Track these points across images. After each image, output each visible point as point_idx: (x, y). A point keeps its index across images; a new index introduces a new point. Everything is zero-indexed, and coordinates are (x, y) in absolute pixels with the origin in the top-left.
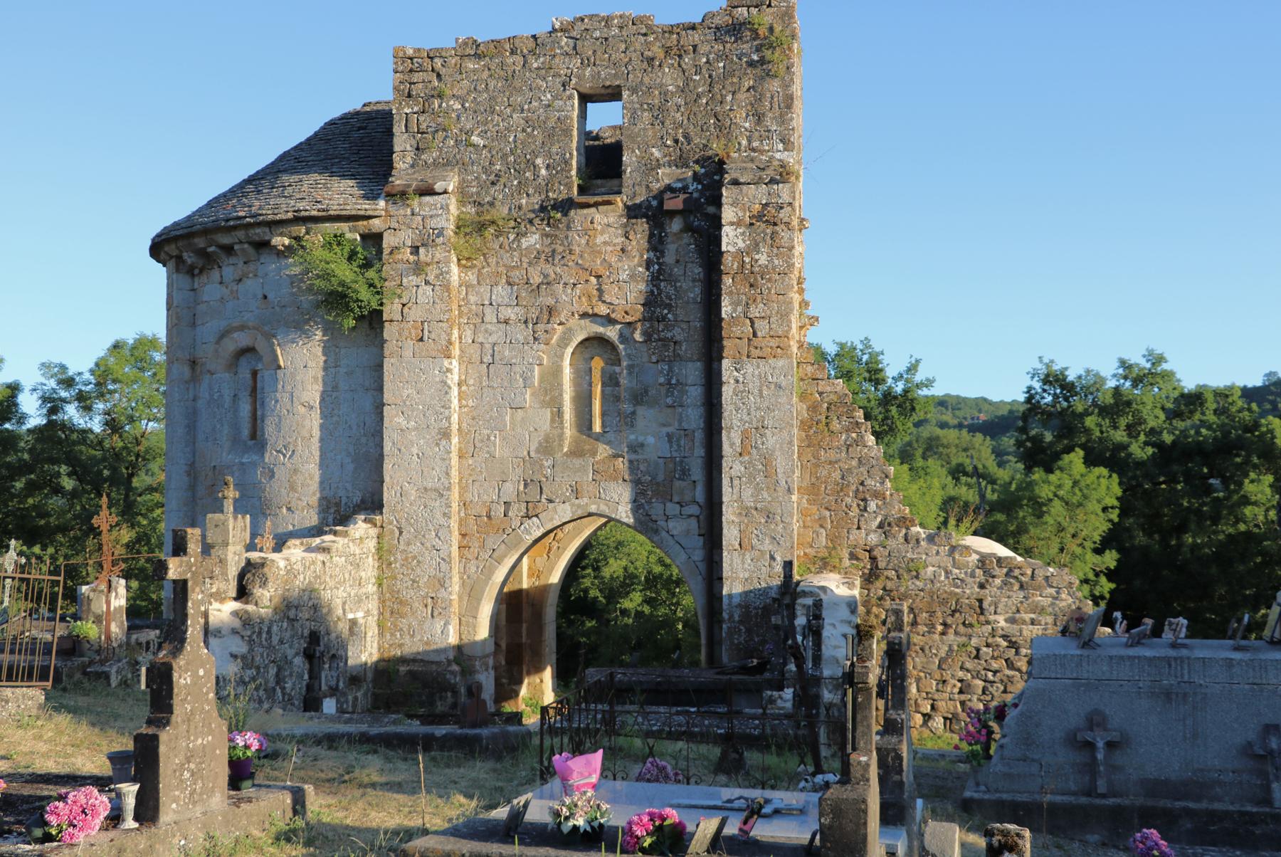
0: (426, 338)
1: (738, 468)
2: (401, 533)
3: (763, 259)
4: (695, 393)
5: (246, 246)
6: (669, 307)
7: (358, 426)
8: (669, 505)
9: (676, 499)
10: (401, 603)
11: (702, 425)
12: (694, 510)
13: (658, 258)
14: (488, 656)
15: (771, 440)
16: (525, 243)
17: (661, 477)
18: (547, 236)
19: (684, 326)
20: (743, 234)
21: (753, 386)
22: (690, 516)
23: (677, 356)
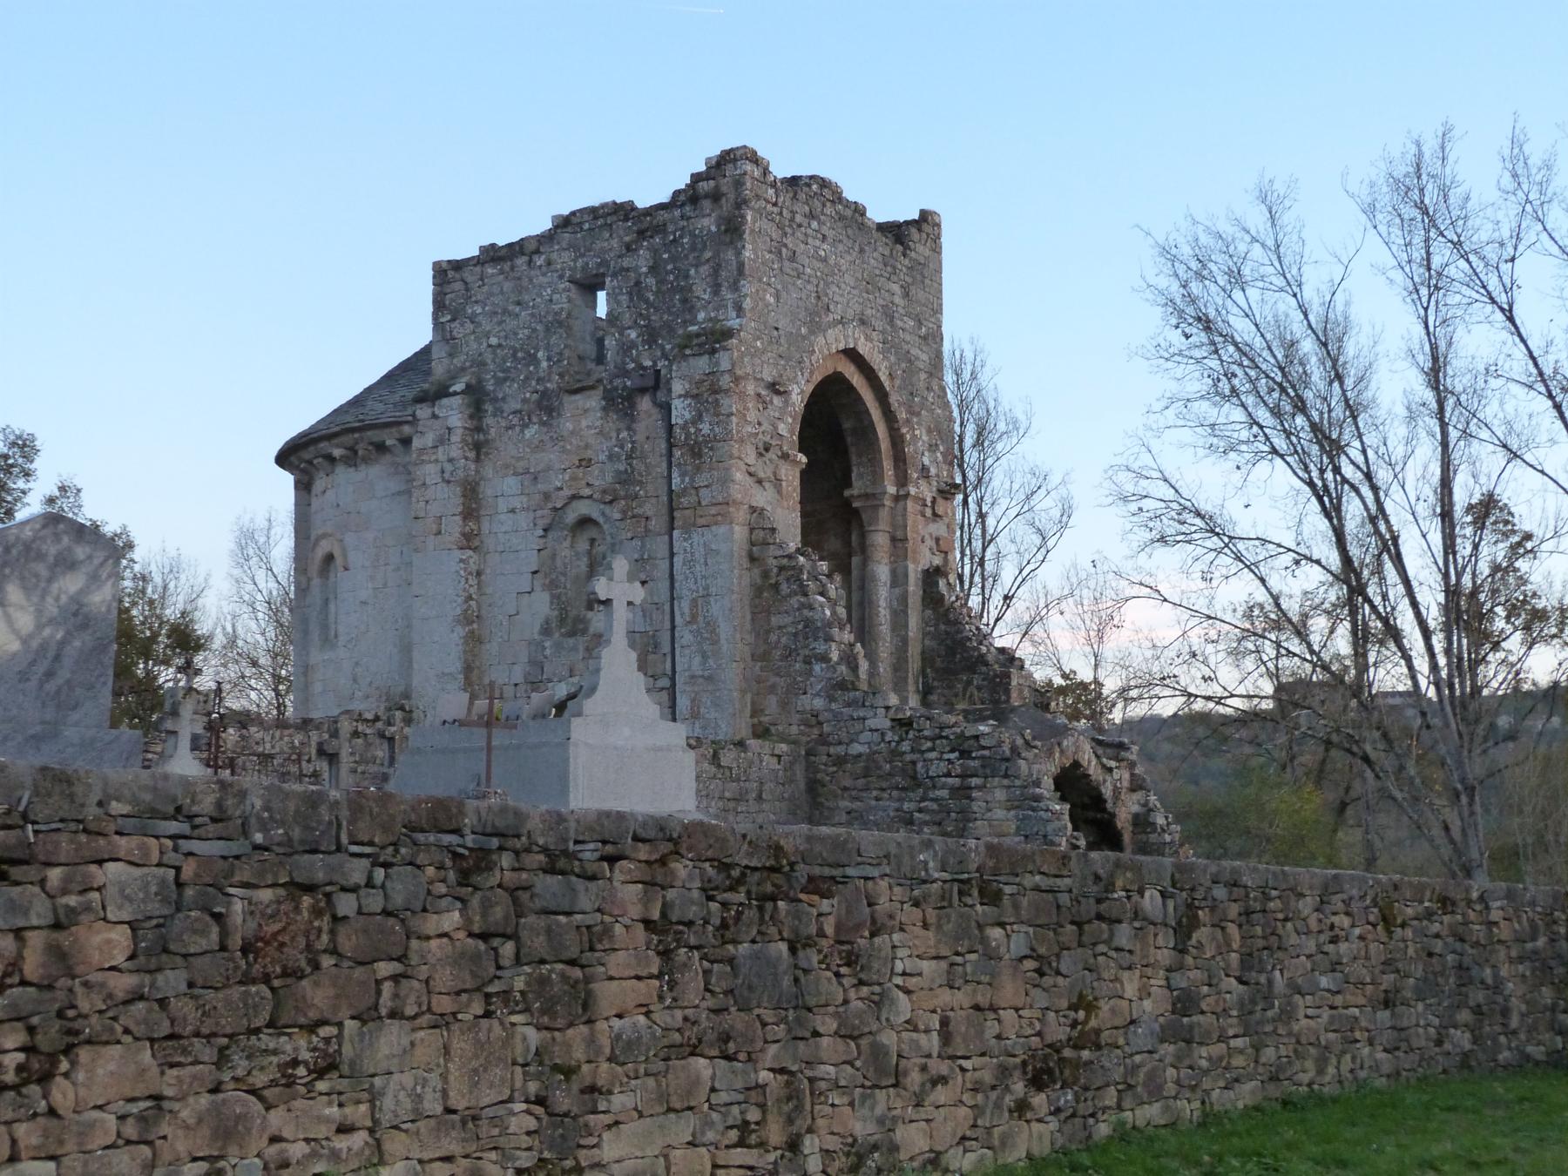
3: (705, 428)
6: (640, 483)
15: (715, 609)
16: (528, 433)
19: (654, 500)
21: (699, 553)
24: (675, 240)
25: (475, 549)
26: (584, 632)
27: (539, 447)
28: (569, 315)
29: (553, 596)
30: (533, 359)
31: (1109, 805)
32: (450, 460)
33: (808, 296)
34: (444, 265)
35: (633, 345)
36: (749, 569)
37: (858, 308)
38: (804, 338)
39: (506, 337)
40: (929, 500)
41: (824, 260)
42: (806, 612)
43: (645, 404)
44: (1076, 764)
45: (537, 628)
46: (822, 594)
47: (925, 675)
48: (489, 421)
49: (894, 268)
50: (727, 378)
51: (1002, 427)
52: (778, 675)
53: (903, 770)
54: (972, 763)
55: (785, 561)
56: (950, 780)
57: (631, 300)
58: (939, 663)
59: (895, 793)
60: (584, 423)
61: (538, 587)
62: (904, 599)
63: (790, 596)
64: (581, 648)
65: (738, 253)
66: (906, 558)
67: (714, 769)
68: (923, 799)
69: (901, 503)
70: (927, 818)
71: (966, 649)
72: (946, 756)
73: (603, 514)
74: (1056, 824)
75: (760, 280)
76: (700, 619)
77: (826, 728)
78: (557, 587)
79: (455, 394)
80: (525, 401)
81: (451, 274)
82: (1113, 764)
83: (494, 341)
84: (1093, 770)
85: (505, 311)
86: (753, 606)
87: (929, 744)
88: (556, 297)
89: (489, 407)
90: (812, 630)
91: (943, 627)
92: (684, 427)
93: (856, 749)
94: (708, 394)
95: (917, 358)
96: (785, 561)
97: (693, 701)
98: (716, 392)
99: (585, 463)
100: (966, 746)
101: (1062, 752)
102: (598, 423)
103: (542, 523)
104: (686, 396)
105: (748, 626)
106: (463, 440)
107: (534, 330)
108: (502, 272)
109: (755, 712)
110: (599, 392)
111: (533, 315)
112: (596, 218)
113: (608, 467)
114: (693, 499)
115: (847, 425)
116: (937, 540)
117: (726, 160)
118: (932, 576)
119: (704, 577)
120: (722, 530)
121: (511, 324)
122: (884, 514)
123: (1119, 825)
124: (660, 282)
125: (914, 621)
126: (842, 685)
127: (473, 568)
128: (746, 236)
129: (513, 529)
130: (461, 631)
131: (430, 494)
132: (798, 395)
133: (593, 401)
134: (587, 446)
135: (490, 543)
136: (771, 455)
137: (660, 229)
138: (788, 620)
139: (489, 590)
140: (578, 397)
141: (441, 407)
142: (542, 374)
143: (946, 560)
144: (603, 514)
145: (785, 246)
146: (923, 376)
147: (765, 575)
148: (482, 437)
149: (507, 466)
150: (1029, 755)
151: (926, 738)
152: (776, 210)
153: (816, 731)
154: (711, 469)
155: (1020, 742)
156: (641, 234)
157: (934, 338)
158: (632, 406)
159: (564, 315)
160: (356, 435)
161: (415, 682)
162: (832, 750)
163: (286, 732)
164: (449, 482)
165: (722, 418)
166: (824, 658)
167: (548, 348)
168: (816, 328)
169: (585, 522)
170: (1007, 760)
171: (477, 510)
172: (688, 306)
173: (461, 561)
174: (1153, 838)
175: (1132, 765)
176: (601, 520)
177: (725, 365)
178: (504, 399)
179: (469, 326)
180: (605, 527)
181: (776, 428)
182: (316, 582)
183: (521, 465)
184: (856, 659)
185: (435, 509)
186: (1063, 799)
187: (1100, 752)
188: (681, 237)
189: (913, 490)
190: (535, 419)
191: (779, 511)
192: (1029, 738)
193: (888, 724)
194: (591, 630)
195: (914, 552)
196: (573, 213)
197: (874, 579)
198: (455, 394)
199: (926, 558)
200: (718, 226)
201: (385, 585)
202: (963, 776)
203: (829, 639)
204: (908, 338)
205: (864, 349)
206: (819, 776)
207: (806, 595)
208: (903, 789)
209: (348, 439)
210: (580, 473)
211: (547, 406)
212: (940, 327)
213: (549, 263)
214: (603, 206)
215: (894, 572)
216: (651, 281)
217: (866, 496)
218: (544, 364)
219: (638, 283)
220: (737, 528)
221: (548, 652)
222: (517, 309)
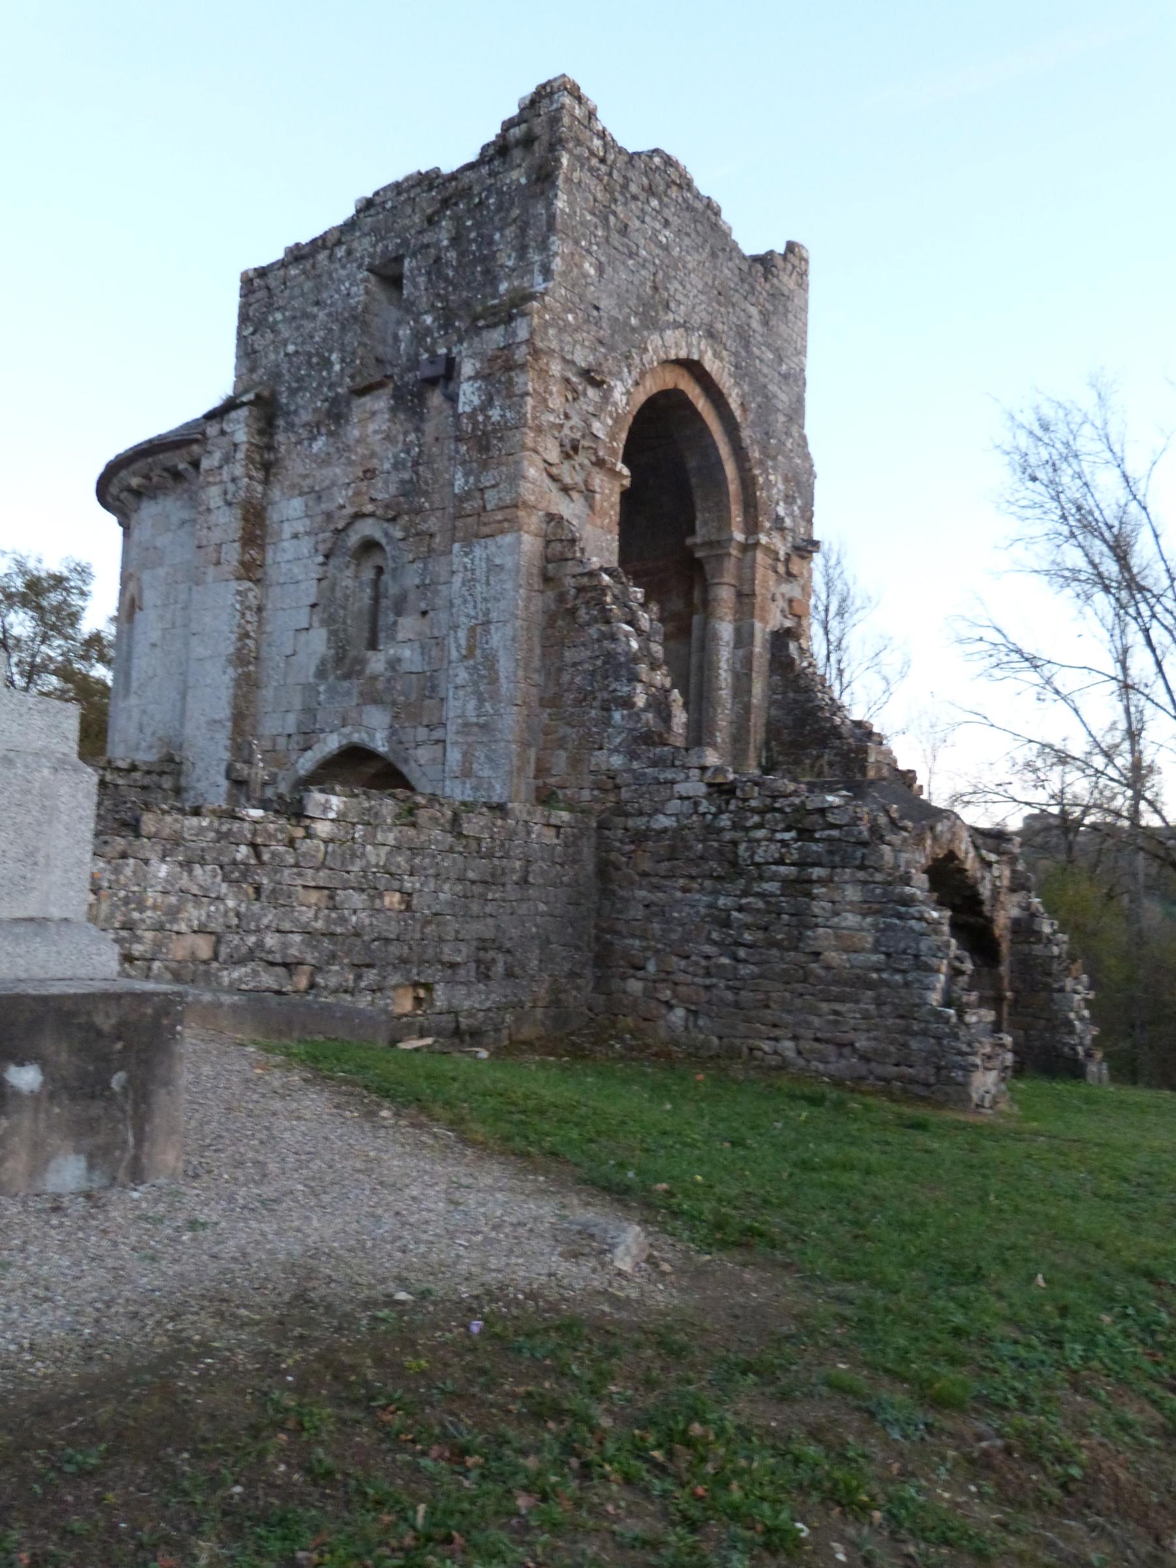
6: (426, 494)
15: (497, 639)
24: (480, 203)
25: (258, 582)
26: (360, 673)
27: (325, 461)
28: (366, 309)
30: (327, 363)
31: (986, 908)
32: (234, 480)
33: (642, 284)
34: (251, 274)
35: (428, 331)
36: (542, 592)
37: (707, 319)
38: (633, 330)
39: (303, 343)
40: (782, 556)
41: (666, 248)
42: (607, 644)
43: (436, 399)
44: (951, 856)
45: (312, 670)
46: (629, 623)
47: (769, 749)
48: (280, 437)
49: (753, 288)
50: (524, 349)
51: (858, 603)
52: (569, 724)
53: (719, 851)
54: (814, 847)
55: (585, 581)
56: (782, 869)
57: (430, 280)
58: (786, 736)
59: (708, 883)
61: (316, 624)
62: (748, 661)
63: (589, 624)
64: (355, 692)
65: (549, 204)
66: (752, 616)
67: (450, 839)
68: (745, 893)
69: (750, 554)
70: (749, 919)
71: (818, 720)
72: (779, 836)
73: (387, 534)
74: (935, 940)
75: (577, 242)
76: (478, 652)
77: (625, 794)
79: (243, 404)
80: (316, 410)
81: (257, 282)
82: (992, 857)
84: (970, 863)
86: (545, 638)
87: (756, 818)
89: (281, 422)
90: (620, 667)
91: (791, 695)
92: (472, 416)
93: (662, 821)
94: (501, 371)
95: (775, 396)
96: (585, 581)
97: (465, 754)
98: (510, 369)
99: (369, 474)
100: (808, 822)
101: (935, 839)
102: (384, 427)
103: (322, 548)
105: (536, 663)
107: (330, 330)
108: (304, 272)
109: (542, 770)
110: (388, 390)
112: (399, 194)
114: (476, 504)
115: (692, 463)
116: (790, 601)
117: (544, 94)
118: (782, 638)
119: (485, 600)
120: (508, 539)
121: (309, 325)
122: (730, 565)
123: (997, 932)
124: (462, 254)
125: (758, 688)
126: (649, 738)
127: (254, 602)
128: (560, 182)
129: (294, 555)
130: (231, 672)
131: (213, 518)
132: (625, 395)
133: (381, 402)
134: (373, 454)
135: (273, 574)
136: (582, 458)
137: (465, 193)
138: (585, 654)
139: (268, 628)
141: (229, 421)
142: (334, 379)
143: (799, 625)
145: (615, 213)
146: (782, 419)
147: (561, 598)
148: (272, 456)
149: (293, 486)
150: (895, 839)
151: (754, 811)
152: (603, 168)
153: (612, 797)
154: (499, 464)
155: (882, 820)
156: (445, 203)
157: (796, 381)
160: (150, 460)
162: (630, 823)
165: (514, 398)
166: (627, 703)
167: (342, 350)
168: (651, 323)
169: (369, 546)
170: (865, 844)
171: (263, 538)
172: (491, 278)
173: (239, 593)
174: (1038, 949)
175: (1013, 860)
176: (383, 541)
177: (523, 334)
179: (270, 336)
180: (388, 548)
181: (589, 426)
184: (668, 707)
185: (216, 536)
186: (941, 904)
187: (980, 841)
188: (487, 198)
189: (763, 539)
190: (323, 430)
191: (589, 527)
192: (895, 815)
193: (702, 789)
194: (368, 672)
195: (763, 609)
196: (377, 194)
197: (716, 637)
198: (243, 404)
199: (776, 619)
200: (528, 178)
201: (174, 625)
202: (801, 864)
203: (634, 678)
204: (765, 370)
205: (711, 364)
206: (613, 856)
207: (608, 622)
208: (719, 878)
209: (139, 465)
211: (336, 415)
212: (802, 370)
213: (349, 253)
214: (407, 179)
215: (738, 631)
217: (710, 544)
218: (337, 367)
219: (438, 260)
220: (526, 538)
221: (322, 697)
222: (315, 310)
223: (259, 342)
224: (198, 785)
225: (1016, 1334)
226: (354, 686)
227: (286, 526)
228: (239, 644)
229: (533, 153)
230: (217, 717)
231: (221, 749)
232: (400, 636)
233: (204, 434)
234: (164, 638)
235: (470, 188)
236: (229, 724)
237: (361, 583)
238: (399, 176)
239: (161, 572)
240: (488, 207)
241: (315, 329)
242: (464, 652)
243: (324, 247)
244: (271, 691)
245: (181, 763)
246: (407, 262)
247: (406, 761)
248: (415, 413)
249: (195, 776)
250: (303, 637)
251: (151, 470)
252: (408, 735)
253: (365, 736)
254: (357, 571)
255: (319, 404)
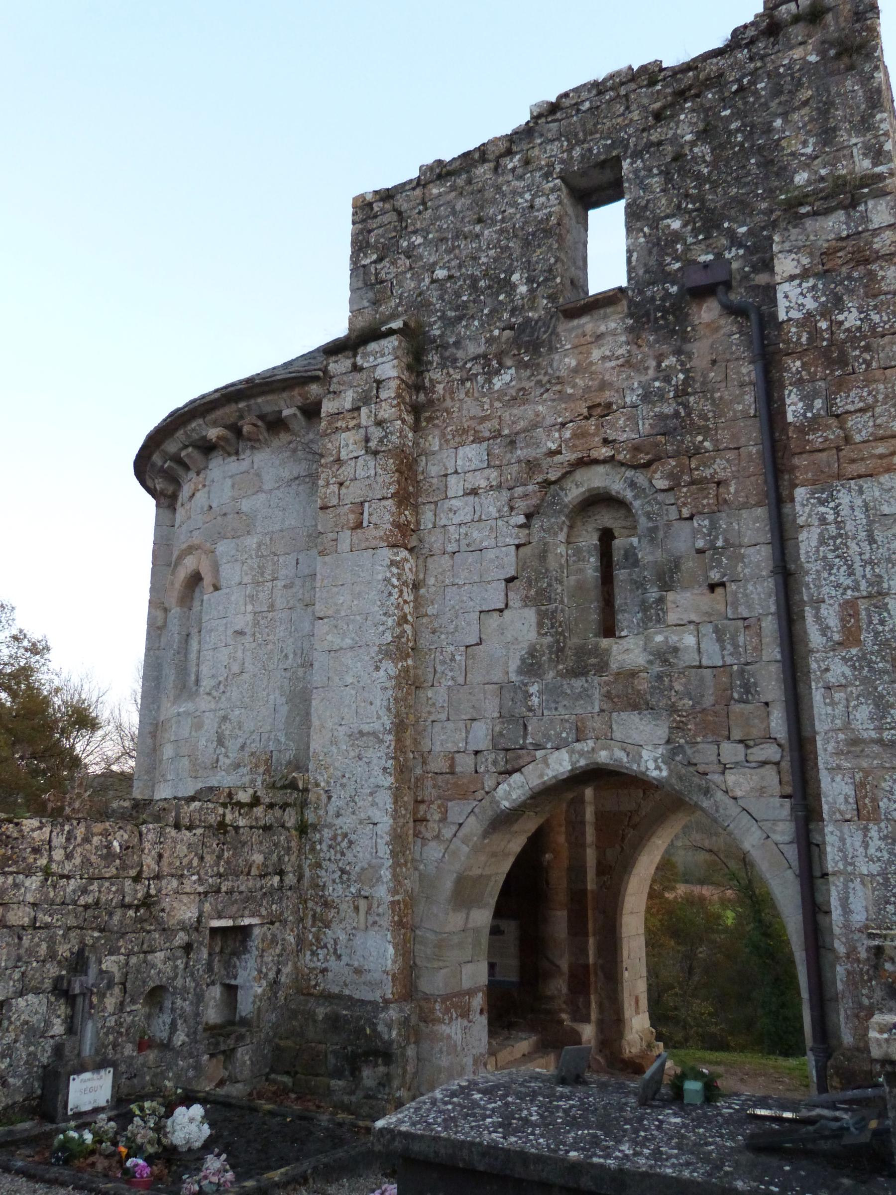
0: (365, 524)
1: (838, 670)
2: (330, 798)
4: (759, 557)
5: (190, 449)
6: (705, 431)
7: (295, 654)
8: (726, 746)
9: (737, 734)
10: (326, 905)
11: (773, 609)
12: (771, 752)
13: (683, 364)
14: (471, 993)
16: (498, 383)
17: (708, 701)
18: (526, 366)
20: (814, 288)
22: (764, 763)
23: (722, 503)
24: (741, 89)
27: (520, 398)
29: (542, 616)
30: (508, 286)
32: (379, 423)
34: (369, 198)
35: (677, 237)
39: (460, 267)
45: (514, 664)
60: (596, 354)
78: (550, 600)
79: (391, 332)
80: (490, 341)
83: (441, 274)
85: (458, 235)
88: (539, 201)
89: (434, 358)
97: (859, 787)
98: (867, 261)
104: (804, 275)
106: (399, 396)
111: (502, 231)
112: (600, 93)
113: (644, 410)
114: (833, 434)
121: (466, 247)
130: (390, 668)
131: (346, 472)
134: (604, 386)
135: (435, 540)
137: (718, 80)
140: (584, 320)
141: (365, 356)
144: (632, 485)
148: (422, 397)
149: (465, 431)
154: (868, 382)
158: (682, 318)
159: (553, 220)
160: (241, 405)
161: (316, 745)
163: (98, 827)
164: (376, 453)
167: (528, 266)
169: (600, 500)
171: (417, 495)
173: (393, 563)
176: (629, 495)
178: (457, 344)
180: (637, 504)
182: (176, 611)
183: (485, 429)
185: (352, 493)
188: (753, 83)
194: (614, 666)
198: (391, 332)
200: (822, 53)
201: (272, 607)
209: (229, 412)
210: (591, 425)
213: (527, 162)
214: (612, 76)
216: (703, 150)
219: (678, 157)
221: (535, 700)
222: (478, 228)
223: (387, 270)
224: (338, 822)
225: (408, 1077)
226: (596, 685)
227: (452, 480)
228: (398, 631)
229: (826, 27)
230: (366, 728)
231: (377, 771)
232: (672, 618)
233: (325, 371)
234: (256, 624)
235: (721, 75)
236: (389, 738)
237: (578, 551)
238: (600, 73)
239: (251, 542)
240: (756, 93)
241: (480, 249)
242: (837, 637)
243: (483, 159)
244: (442, 691)
245: (306, 790)
246: (626, 164)
247: (707, 792)
248: (673, 332)
249: (332, 809)
250: (494, 620)
251: (241, 417)
252: (705, 754)
253: (620, 754)
254: (568, 536)
255: (496, 332)
